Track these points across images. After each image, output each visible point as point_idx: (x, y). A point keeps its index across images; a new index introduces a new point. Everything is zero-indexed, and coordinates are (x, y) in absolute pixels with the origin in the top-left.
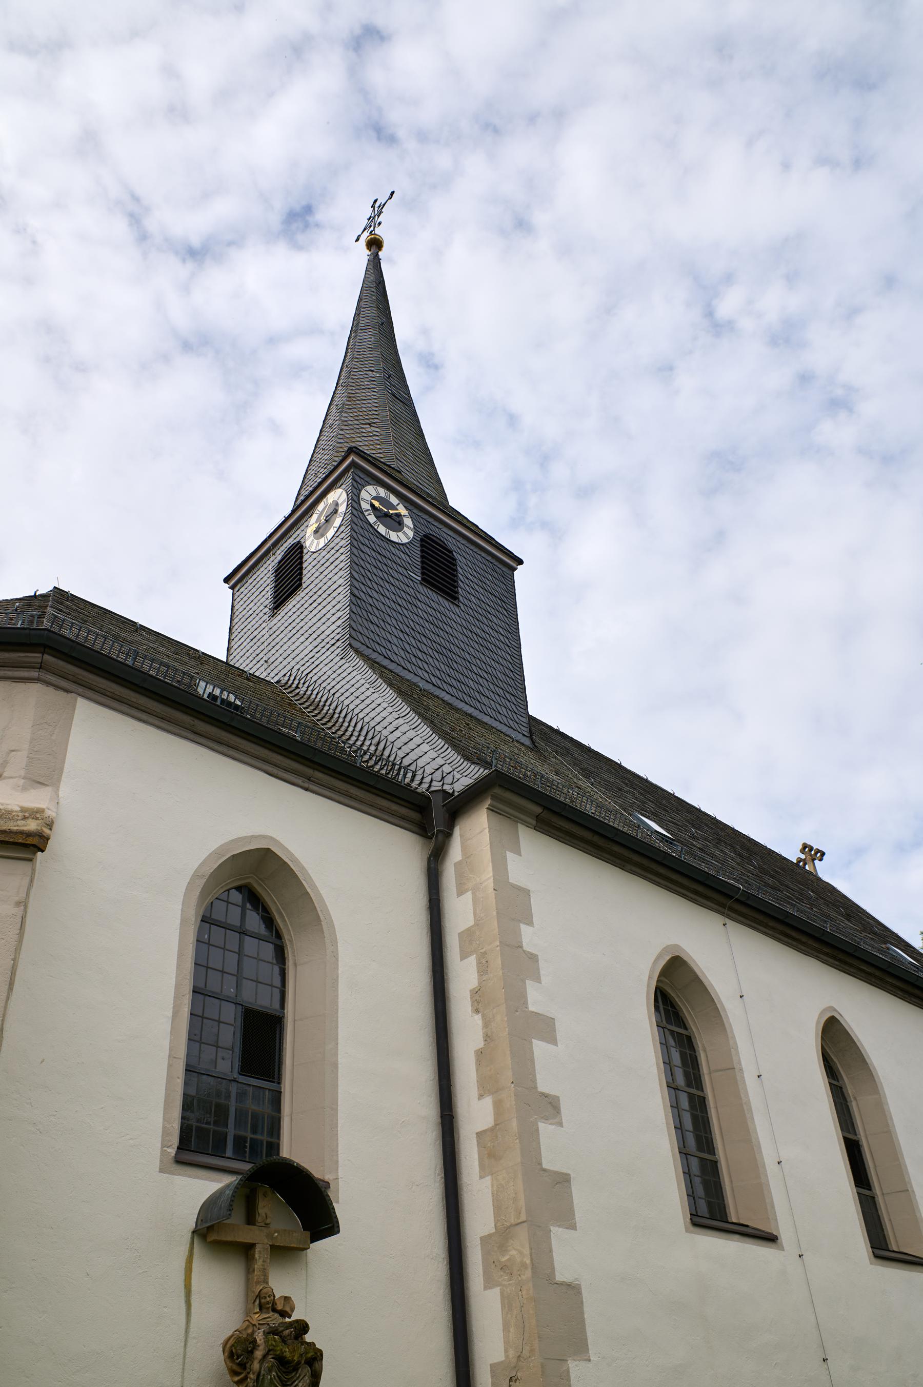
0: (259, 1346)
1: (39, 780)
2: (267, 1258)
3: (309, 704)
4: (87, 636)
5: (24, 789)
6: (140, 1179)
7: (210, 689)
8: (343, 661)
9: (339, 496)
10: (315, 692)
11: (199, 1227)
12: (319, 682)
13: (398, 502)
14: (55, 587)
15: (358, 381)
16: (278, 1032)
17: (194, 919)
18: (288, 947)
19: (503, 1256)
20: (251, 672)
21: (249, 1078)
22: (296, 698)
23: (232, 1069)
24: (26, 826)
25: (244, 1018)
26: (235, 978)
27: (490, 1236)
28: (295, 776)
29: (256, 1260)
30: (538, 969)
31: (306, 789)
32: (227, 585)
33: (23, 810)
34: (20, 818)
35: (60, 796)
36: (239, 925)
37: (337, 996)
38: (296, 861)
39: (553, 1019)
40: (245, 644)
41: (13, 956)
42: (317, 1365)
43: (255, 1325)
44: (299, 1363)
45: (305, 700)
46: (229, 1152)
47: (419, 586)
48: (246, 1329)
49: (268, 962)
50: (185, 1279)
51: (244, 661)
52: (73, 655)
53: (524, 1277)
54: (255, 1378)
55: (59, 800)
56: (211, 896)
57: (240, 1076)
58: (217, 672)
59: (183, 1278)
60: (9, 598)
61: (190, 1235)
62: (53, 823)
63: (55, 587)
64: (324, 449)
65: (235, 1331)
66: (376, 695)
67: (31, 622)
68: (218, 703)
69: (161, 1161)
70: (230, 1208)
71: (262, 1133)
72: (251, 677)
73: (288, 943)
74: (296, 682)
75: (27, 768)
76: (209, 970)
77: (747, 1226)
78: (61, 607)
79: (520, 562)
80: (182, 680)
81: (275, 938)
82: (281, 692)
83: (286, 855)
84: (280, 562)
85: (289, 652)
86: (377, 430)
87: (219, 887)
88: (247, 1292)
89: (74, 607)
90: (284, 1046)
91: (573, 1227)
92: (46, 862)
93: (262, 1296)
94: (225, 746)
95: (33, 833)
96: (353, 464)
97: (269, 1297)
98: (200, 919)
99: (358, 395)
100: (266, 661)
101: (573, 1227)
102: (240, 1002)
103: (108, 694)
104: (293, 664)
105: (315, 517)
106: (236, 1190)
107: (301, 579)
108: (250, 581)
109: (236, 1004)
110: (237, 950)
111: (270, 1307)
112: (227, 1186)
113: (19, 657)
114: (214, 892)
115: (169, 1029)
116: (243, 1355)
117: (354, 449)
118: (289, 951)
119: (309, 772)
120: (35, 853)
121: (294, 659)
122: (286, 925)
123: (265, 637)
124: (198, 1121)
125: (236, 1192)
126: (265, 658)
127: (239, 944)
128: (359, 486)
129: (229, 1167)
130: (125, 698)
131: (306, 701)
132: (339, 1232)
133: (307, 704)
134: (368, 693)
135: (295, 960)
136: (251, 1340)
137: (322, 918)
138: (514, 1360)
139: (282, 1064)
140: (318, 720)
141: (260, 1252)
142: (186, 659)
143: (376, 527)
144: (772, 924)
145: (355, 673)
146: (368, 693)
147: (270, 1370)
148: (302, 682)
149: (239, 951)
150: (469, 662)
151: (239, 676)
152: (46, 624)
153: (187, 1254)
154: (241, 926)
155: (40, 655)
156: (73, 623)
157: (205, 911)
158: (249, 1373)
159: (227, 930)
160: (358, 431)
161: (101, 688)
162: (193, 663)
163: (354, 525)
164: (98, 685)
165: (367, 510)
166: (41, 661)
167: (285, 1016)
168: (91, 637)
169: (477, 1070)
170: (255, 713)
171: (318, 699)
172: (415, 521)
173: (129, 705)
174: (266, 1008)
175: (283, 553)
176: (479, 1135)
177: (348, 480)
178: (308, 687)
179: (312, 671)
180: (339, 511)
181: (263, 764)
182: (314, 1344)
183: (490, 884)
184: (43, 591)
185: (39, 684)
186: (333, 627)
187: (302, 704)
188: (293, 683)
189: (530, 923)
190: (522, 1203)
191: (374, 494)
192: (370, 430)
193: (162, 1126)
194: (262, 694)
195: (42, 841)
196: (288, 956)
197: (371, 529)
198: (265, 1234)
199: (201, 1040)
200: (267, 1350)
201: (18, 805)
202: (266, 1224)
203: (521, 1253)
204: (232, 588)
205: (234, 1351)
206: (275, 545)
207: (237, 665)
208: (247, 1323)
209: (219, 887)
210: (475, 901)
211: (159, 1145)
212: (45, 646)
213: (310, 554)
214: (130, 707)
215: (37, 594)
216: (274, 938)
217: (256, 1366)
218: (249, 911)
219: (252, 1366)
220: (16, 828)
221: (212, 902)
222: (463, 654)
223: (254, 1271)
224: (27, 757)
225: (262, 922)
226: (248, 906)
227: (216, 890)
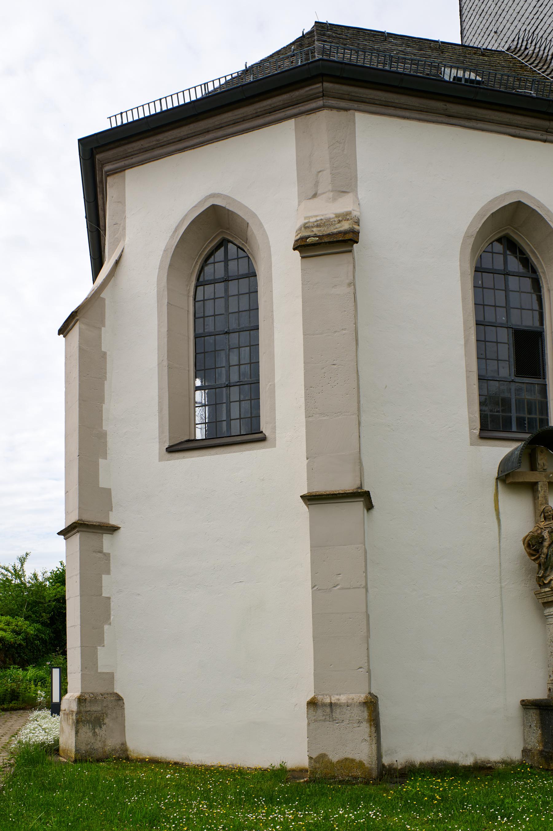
0: (546, 539)
1: (342, 190)
2: (547, 490)
3: (538, 61)
4: (351, 57)
5: (334, 199)
6: (459, 451)
7: (454, 71)
10: (542, 48)
11: (500, 476)
12: (545, 36)
14: (316, 22)
16: (540, 343)
17: (469, 271)
18: (542, 278)
20: (484, 47)
21: (522, 378)
22: (526, 60)
23: (510, 374)
24: (342, 227)
25: (515, 337)
26: (505, 309)
28: (535, 131)
29: (539, 492)
31: (545, 141)
33: (337, 216)
34: (336, 222)
35: (359, 199)
36: (503, 268)
38: (542, 206)
40: (475, 21)
41: (354, 321)
43: (542, 528)
45: (534, 59)
46: (514, 428)
48: (536, 531)
49: (528, 293)
50: (495, 506)
51: (477, 39)
52: (344, 75)
54: (545, 557)
55: (359, 201)
56: (479, 251)
57: (516, 378)
58: (457, 56)
59: (494, 505)
60: (285, 45)
61: (494, 481)
62: (359, 220)
63: (316, 22)
65: (530, 532)
67: (307, 59)
68: (463, 82)
69: (470, 439)
70: (520, 462)
72: (485, 52)
73: (541, 274)
75: (332, 182)
76: (485, 307)
78: (325, 38)
80: (430, 73)
81: (531, 272)
82: (512, 58)
83: (534, 203)
85: (514, 15)
87: (484, 242)
88: (535, 510)
89: (334, 35)
90: (546, 352)
92: (361, 251)
93: (545, 512)
94: (474, 121)
95: (348, 231)
97: (550, 512)
98: (473, 270)
100: (496, 32)
102: (510, 326)
103: (377, 102)
106: (522, 450)
109: (507, 328)
110: (504, 288)
111: (551, 518)
112: (516, 449)
113: (307, 91)
114: (482, 247)
115: (464, 353)
116: (536, 545)
118: (543, 281)
120: (352, 246)
121: (520, 21)
123: (492, 8)
124: (491, 411)
125: (522, 452)
127: (505, 283)
129: (515, 437)
130: (390, 102)
131: (535, 60)
133: (536, 62)
135: (549, 287)
136: (540, 536)
139: (545, 365)
140: (548, 75)
141: (541, 487)
142: (429, 52)
148: (529, 41)
149: (506, 288)
151: (475, 54)
152: (318, 56)
153: (494, 491)
154: (504, 269)
156: (338, 47)
157: (476, 264)
158: (541, 554)
159: (495, 275)
161: (370, 99)
162: (435, 54)
164: (368, 97)
166: (322, 90)
167: (545, 330)
168: (354, 57)
170: (494, 84)
171: (545, 54)
173: (394, 107)
174: (518, 326)
178: (536, 45)
179: (537, 27)
181: (507, 127)
184: (308, 29)
185: (325, 111)
187: (532, 63)
188: (522, 46)
193: (468, 417)
194: (497, 65)
195: (355, 235)
196: (543, 285)
198: (544, 476)
199: (486, 358)
200: (551, 541)
201: (333, 213)
202: (544, 470)
205: (530, 543)
207: (471, 45)
208: (537, 527)
209: (484, 242)
211: (468, 429)
212: (322, 75)
214: (395, 109)
215: (304, 34)
216: (530, 273)
217: (545, 550)
218: (510, 256)
219: (542, 551)
220: (335, 231)
221: (481, 256)
223: (538, 498)
224: (331, 174)
225: (519, 263)
226: (508, 252)
227: (482, 245)
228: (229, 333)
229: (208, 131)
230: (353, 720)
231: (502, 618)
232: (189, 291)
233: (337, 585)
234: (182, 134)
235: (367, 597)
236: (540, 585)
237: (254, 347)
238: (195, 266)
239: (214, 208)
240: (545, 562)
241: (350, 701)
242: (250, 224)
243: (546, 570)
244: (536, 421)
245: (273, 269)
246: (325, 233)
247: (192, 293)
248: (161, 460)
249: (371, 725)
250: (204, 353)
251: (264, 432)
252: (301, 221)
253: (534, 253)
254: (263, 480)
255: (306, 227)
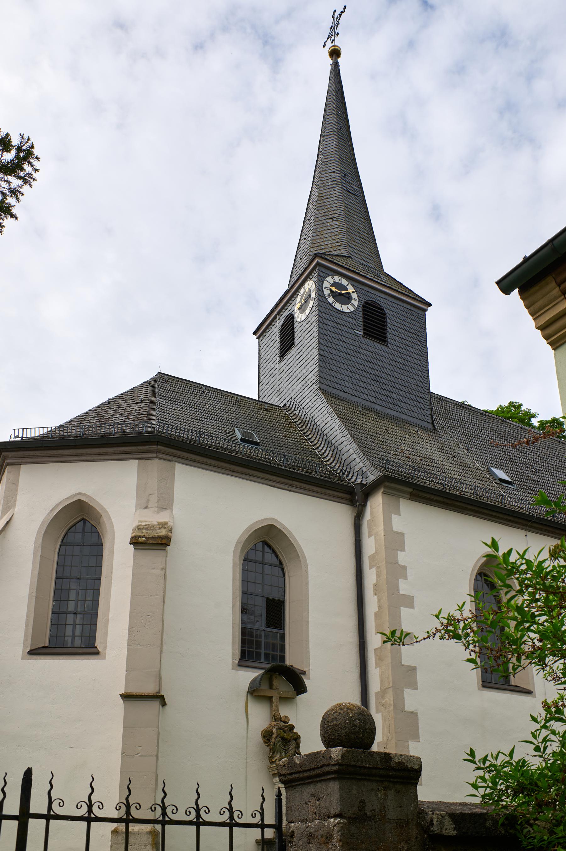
5: (158, 512)
8: (316, 397)
9: (310, 285)
10: (303, 414)
13: (347, 283)
14: (158, 372)
15: (325, 182)
19: (383, 700)
27: (378, 692)
30: (406, 573)
31: (290, 491)
32: (255, 337)
33: (159, 524)
37: (308, 591)
39: (413, 597)
40: (267, 377)
42: (298, 741)
44: (290, 740)
46: (263, 660)
47: (362, 338)
53: (390, 709)
61: (246, 693)
64: (305, 239)
66: (332, 421)
70: (260, 684)
71: (277, 652)
74: (294, 406)
77: (519, 687)
79: (430, 305)
84: (282, 326)
86: (337, 223)
91: (417, 689)
96: (318, 264)
99: (324, 194)
100: (278, 391)
101: (417, 689)
104: (292, 394)
105: (299, 297)
107: (293, 339)
108: (268, 335)
115: (231, 612)
117: (318, 254)
119: (291, 482)
120: (166, 547)
122: (284, 558)
126: (278, 389)
128: (322, 278)
132: (307, 692)
134: (328, 419)
137: (300, 555)
138: (386, 741)
143: (333, 305)
144: (558, 532)
145: (322, 406)
146: (328, 419)
147: (279, 742)
150: (394, 382)
155: (155, 446)
157: (245, 555)
160: (325, 225)
163: (320, 307)
165: (328, 295)
169: (375, 622)
171: (305, 419)
172: (358, 293)
175: (284, 319)
176: (375, 650)
177: (315, 275)
178: (300, 410)
180: (312, 297)
182: (297, 733)
183: (382, 533)
186: (311, 375)
188: (292, 407)
189: (403, 550)
190: (391, 679)
191: (332, 282)
192: (332, 224)
197: (331, 308)
203: (390, 699)
204: (258, 338)
206: (279, 313)
210: (375, 539)
211: (231, 659)
213: (297, 323)
217: (273, 740)
220: (157, 535)
222: (389, 377)
228: (80, 579)
229: (82, 455)
230: (141, 844)
231: (246, 784)
232: (55, 548)
233: (139, 753)
234: (64, 453)
235: (157, 762)
236: (270, 763)
237: (97, 591)
238: (61, 533)
239: (79, 501)
240: (273, 748)
241: (140, 831)
242: (103, 516)
243: (274, 753)
244: (277, 656)
245: (115, 546)
246: (151, 535)
247: (57, 550)
248: (23, 658)
249: (153, 847)
250: (61, 589)
251: (98, 648)
252: (136, 524)
253: (281, 554)
254: (94, 680)
255: (139, 528)
